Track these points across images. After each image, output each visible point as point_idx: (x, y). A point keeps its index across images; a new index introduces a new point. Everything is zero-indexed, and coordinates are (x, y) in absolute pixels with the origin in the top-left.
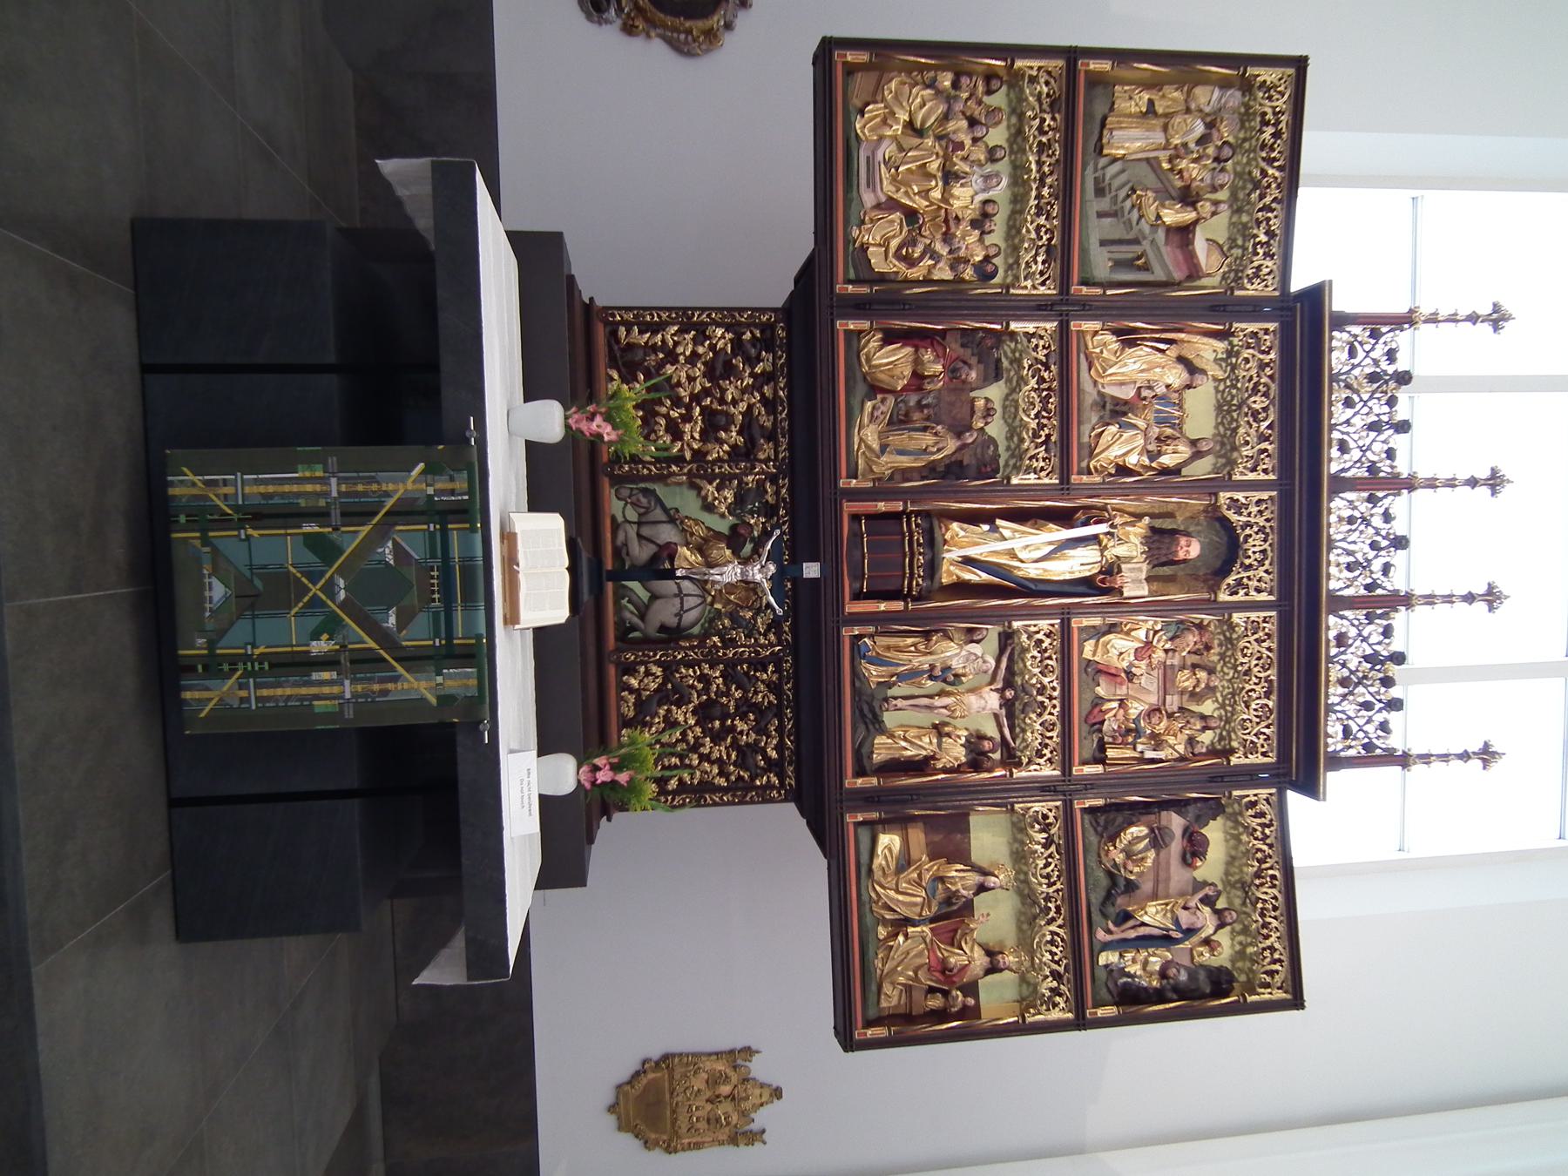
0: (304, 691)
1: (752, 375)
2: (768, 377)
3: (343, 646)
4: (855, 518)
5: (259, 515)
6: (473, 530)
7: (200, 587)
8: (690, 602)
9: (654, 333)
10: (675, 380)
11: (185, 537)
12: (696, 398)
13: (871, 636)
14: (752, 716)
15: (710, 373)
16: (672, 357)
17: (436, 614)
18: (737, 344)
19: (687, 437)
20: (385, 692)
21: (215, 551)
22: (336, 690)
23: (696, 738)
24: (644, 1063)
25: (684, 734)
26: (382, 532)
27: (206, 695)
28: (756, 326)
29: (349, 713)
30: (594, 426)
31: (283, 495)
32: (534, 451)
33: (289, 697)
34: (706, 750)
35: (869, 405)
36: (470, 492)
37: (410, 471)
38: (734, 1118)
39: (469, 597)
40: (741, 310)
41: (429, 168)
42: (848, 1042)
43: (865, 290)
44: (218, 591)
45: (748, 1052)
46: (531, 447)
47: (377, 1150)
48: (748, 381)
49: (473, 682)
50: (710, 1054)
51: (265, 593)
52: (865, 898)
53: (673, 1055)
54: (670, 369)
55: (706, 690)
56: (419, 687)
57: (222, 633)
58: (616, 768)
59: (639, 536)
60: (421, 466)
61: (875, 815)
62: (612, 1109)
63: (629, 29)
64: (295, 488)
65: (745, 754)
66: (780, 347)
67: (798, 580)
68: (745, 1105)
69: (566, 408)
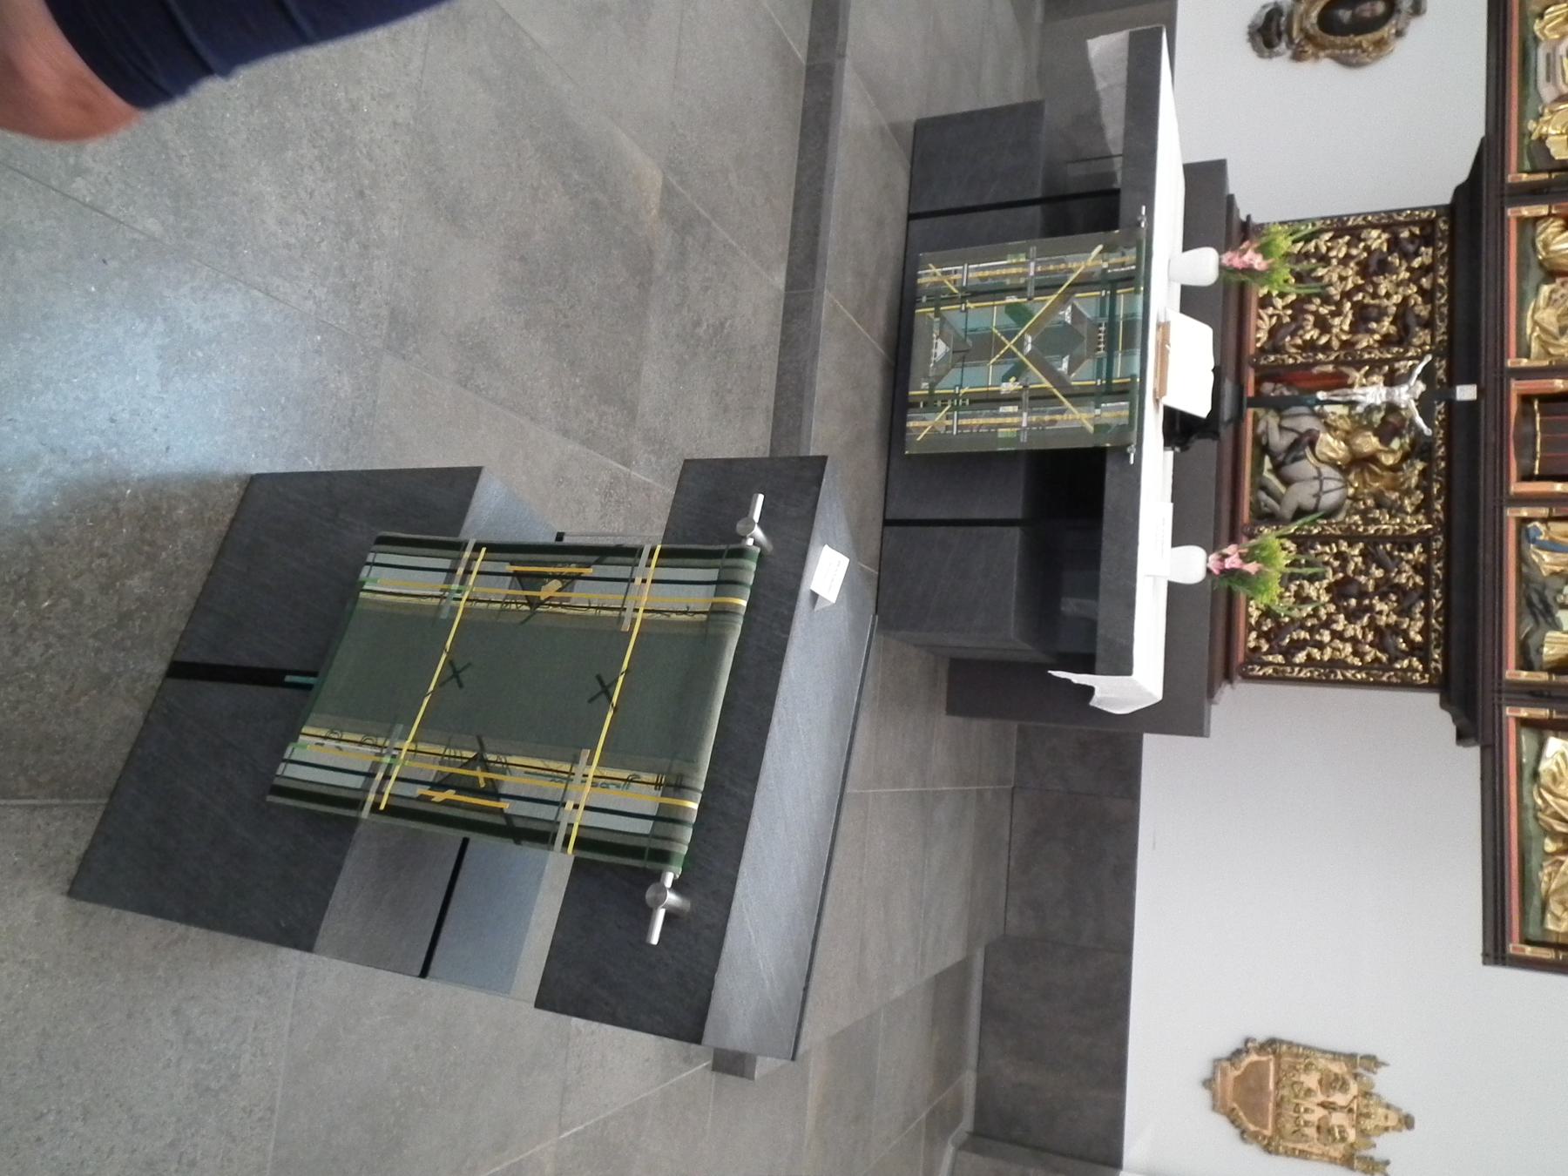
0: (993, 421)
1: (1409, 269)
2: (1426, 270)
4: (1526, 399)
5: (975, 293)
6: (1137, 292)
7: (930, 345)
10: (1326, 280)
11: (924, 311)
12: (1347, 295)
13: (1544, 521)
14: (1394, 598)
15: (1364, 270)
16: (1324, 260)
17: (1100, 361)
18: (1394, 244)
19: (1335, 330)
20: (1053, 422)
21: (943, 320)
22: (1016, 420)
23: (1329, 615)
24: (1247, 1041)
25: (1316, 610)
26: (1064, 300)
27: (923, 424)
28: (1414, 223)
29: (1024, 438)
30: (1246, 258)
31: (994, 277)
33: (981, 426)
34: (1339, 627)
35: (1545, 289)
36: (1138, 263)
37: (1090, 251)
38: (1352, 1135)
39: (1129, 344)
40: (1399, 212)
41: (1125, 45)
42: (1496, 952)
43: (1544, 176)
44: (941, 349)
45: (1372, 1062)
47: (972, 1059)
48: (1404, 275)
49: (1126, 413)
50: (1324, 1052)
51: (973, 349)
52: (1527, 801)
53: (1282, 1042)
55: (1343, 568)
56: (1080, 420)
57: (939, 378)
58: (1245, 558)
59: (1281, 428)
60: (1100, 247)
61: (1543, 713)
62: (1208, 1083)
63: (1298, 56)
65: (1382, 636)
66: (1441, 239)
67: (1452, 405)
68: (1368, 1124)
69: (1220, 253)
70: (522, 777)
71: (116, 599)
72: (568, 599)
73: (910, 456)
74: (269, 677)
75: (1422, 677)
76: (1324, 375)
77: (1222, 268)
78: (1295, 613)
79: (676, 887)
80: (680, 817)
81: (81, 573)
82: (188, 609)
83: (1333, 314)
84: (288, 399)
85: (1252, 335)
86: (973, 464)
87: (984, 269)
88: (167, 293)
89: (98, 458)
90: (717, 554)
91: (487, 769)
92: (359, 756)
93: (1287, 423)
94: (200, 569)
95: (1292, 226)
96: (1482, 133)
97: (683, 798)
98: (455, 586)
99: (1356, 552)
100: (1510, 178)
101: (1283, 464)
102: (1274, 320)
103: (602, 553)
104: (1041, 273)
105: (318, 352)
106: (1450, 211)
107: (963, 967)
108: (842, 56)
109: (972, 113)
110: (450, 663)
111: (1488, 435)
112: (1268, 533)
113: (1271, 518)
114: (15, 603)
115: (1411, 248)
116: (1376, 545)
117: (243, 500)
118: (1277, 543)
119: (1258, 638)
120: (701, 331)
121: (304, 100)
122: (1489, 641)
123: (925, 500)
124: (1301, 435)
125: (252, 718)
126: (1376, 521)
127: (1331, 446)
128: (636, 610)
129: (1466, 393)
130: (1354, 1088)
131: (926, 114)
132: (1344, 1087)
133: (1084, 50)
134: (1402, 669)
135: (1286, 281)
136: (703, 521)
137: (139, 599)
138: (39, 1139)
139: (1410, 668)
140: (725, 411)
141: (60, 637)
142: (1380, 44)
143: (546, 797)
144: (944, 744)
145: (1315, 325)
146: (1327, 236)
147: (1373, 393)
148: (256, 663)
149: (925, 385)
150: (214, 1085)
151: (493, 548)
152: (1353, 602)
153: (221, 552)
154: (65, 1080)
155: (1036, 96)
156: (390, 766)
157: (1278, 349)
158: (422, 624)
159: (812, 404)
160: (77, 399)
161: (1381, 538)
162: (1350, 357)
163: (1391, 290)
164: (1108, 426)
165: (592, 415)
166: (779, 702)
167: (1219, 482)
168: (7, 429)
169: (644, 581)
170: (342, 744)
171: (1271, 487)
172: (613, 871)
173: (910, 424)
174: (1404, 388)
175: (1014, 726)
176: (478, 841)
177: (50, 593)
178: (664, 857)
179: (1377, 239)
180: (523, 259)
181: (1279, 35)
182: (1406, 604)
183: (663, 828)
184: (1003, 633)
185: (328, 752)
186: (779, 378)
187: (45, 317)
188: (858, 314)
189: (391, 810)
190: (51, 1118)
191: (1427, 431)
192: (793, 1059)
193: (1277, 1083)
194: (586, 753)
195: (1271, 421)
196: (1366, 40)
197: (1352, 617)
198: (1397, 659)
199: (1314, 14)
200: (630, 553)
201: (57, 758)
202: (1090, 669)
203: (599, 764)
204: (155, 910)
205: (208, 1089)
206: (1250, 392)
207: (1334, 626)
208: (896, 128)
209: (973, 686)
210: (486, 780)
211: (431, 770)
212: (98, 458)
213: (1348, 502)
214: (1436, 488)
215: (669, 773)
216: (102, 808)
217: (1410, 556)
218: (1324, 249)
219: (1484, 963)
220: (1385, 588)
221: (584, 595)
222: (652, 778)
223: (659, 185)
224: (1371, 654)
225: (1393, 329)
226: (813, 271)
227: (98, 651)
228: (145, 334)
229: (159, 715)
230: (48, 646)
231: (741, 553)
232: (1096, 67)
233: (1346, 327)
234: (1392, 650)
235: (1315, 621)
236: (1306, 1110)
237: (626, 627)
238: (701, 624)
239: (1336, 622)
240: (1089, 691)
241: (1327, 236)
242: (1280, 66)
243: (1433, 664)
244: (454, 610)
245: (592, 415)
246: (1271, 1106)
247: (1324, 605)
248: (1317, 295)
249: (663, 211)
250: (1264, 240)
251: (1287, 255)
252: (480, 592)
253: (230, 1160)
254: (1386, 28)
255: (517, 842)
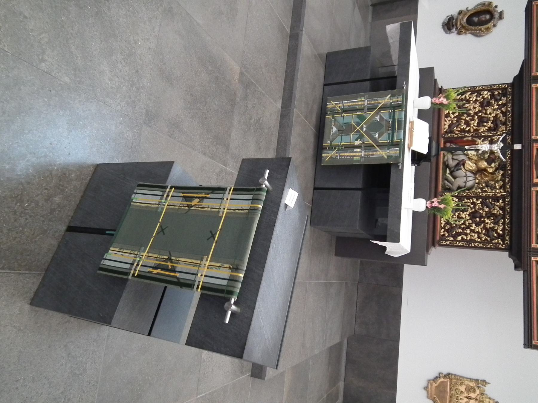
0: (352, 154)
2: (504, 105)
3: (363, 142)
6: (402, 111)
8: (469, 179)
9: (462, 95)
10: (469, 108)
11: (329, 117)
12: (476, 113)
15: (482, 105)
16: (468, 101)
17: (389, 134)
18: (493, 96)
19: (472, 126)
20: (373, 155)
21: (335, 120)
22: (360, 154)
24: (440, 374)
26: (377, 113)
27: (328, 155)
28: (499, 89)
29: (363, 160)
30: (440, 100)
31: (353, 105)
32: (415, 214)
33: (348, 156)
34: (473, 228)
36: (403, 101)
39: (399, 129)
40: (494, 85)
41: (399, 28)
44: (334, 129)
45: (484, 382)
46: (414, 212)
48: (496, 107)
50: (467, 378)
53: (452, 374)
54: (467, 105)
55: (474, 207)
56: (382, 154)
59: (453, 159)
60: (390, 95)
62: (426, 388)
63: (459, 33)
64: (356, 103)
65: (488, 231)
67: (513, 151)
69: (432, 98)
70: (183, 265)
71: (50, 204)
72: (201, 205)
73: (323, 166)
74: (101, 232)
75: (503, 246)
76: (468, 141)
77: (432, 103)
78: (457, 223)
79: (235, 303)
80: (237, 279)
81: (38, 195)
82: (75, 208)
83: (471, 120)
84: (110, 139)
85: (443, 127)
86: (346, 169)
87: (349, 102)
88: (71, 102)
89: (46, 156)
90: (252, 190)
91: (172, 262)
92: (129, 258)
93: (454, 157)
94: (79, 195)
95: (456, 90)
96: (524, 59)
97: (238, 273)
98: (163, 201)
99: (479, 202)
100: (533, 74)
101: (453, 171)
102: (450, 122)
103: (213, 190)
104: (369, 104)
105: (121, 123)
106: (512, 85)
107: (340, 344)
108: (302, 30)
109: (346, 50)
110: (161, 226)
111: (526, 163)
112: (448, 195)
113: (449, 190)
114: (16, 204)
115: (498, 98)
116: (486, 199)
117: (94, 173)
118: (451, 198)
119: (444, 231)
120: (251, 121)
121: (119, 40)
122: (526, 233)
123: (327, 180)
124: (460, 161)
125: (94, 250)
126: (486, 191)
127: (470, 165)
128: (224, 209)
129: (518, 147)
130: (478, 392)
131: (330, 51)
132: (474, 391)
133: (385, 28)
134: (495, 243)
135: (455, 108)
136: (248, 179)
137: (58, 204)
138: (17, 388)
139: (498, 243)
140: (260, 148)
141: (31, 216)
142: (488, 29)
143: (191, 272)
144: (334, 266)
145: (465, 124)
146: (469, 93)
147: (485, 147)
148: (96, 226)
149: (329, 142)
150: (78, 373)
151: (176, 188)
152: (478, 219)
153: (86, 190)
154: (27, 368)
155: (368, 45)
156: (139, 261)
157: (452, 132)
158: (151, 213)
159: (289, 147)
160: (40, 136)
161: (488, 197)
162: (477, 135)
163: (491, 112)
164: (392, 156)
165: (214, 149)
166: (273, 241)
167: (431, 178)
168: (16, 145)
169: (227, 199)
170: (123, 254)
171: (449, 179)
172: (213, 298)
173: (323, 155)
174: (496, 145)
175: (359, 260)
176: (169, 286)
177: (28, 201)
178: (231, 293)
179: (486, 94)
180: (192, 95)
181: (453, 26)
182: (497, 220)
183: (231, 283)
184: (354, 227)
185: (118, 256)
186: (278, 139)
187: (30, 109)
188: (306, 117)
189: (139, 276)
190: (22, 381)
191: (504, 160)
192: (276, 369)
193: (451, 389)
194: (206, 257)
195: (450, 156)
196: (483, 28)
197: (477, 225)
198: (493, 240)
199: (465, 19)
200: (222, 190)
201: (28, 257)
202: (385, 241)
203: (210, 261)
204: (58, 309)
205: (76, 374)
206: (442, 146)
207: (471, 228)
208: (320, 55)
209: (345, 246)
210: (171, 266)
211: (153, 262)
212: (46, 156)
213: (476, 185)
214: (507, 180)
215: (233, 264)
216: (43, 275)
217: (498, 204)
218: (468, 98)
219: (524, 348)
220: (489, 215)
221: (207, 204)
222: (228, 266)
223: (239, 72)
224: (484, 238)
225: (492, 125)
226: (291, 102)
227: (43, 221)
228: (63, 115)
229: (63, 244)
230: (26, 219)
231: (260, 190)
232: (389, 35)
233: (476, 125)
234: (492, 236)
235: (464, 226)
236: (461, 399)
237: (221, 214)
238: (246, 213)
239: (472, 226)
240: (385, 248)
241: (469, 93)
242: (453, 36)
243: (506, 242)
244: (163, 209)
245: (214, 149)
246: (448, 397)
247: (467, 220)
248: (466, 113)
249: (239, 81)
250: (447, 94)
251: (455, 100)
252: (172, 203)
253: (82, 399)
254: (490, 24)
255: (181, 287)
